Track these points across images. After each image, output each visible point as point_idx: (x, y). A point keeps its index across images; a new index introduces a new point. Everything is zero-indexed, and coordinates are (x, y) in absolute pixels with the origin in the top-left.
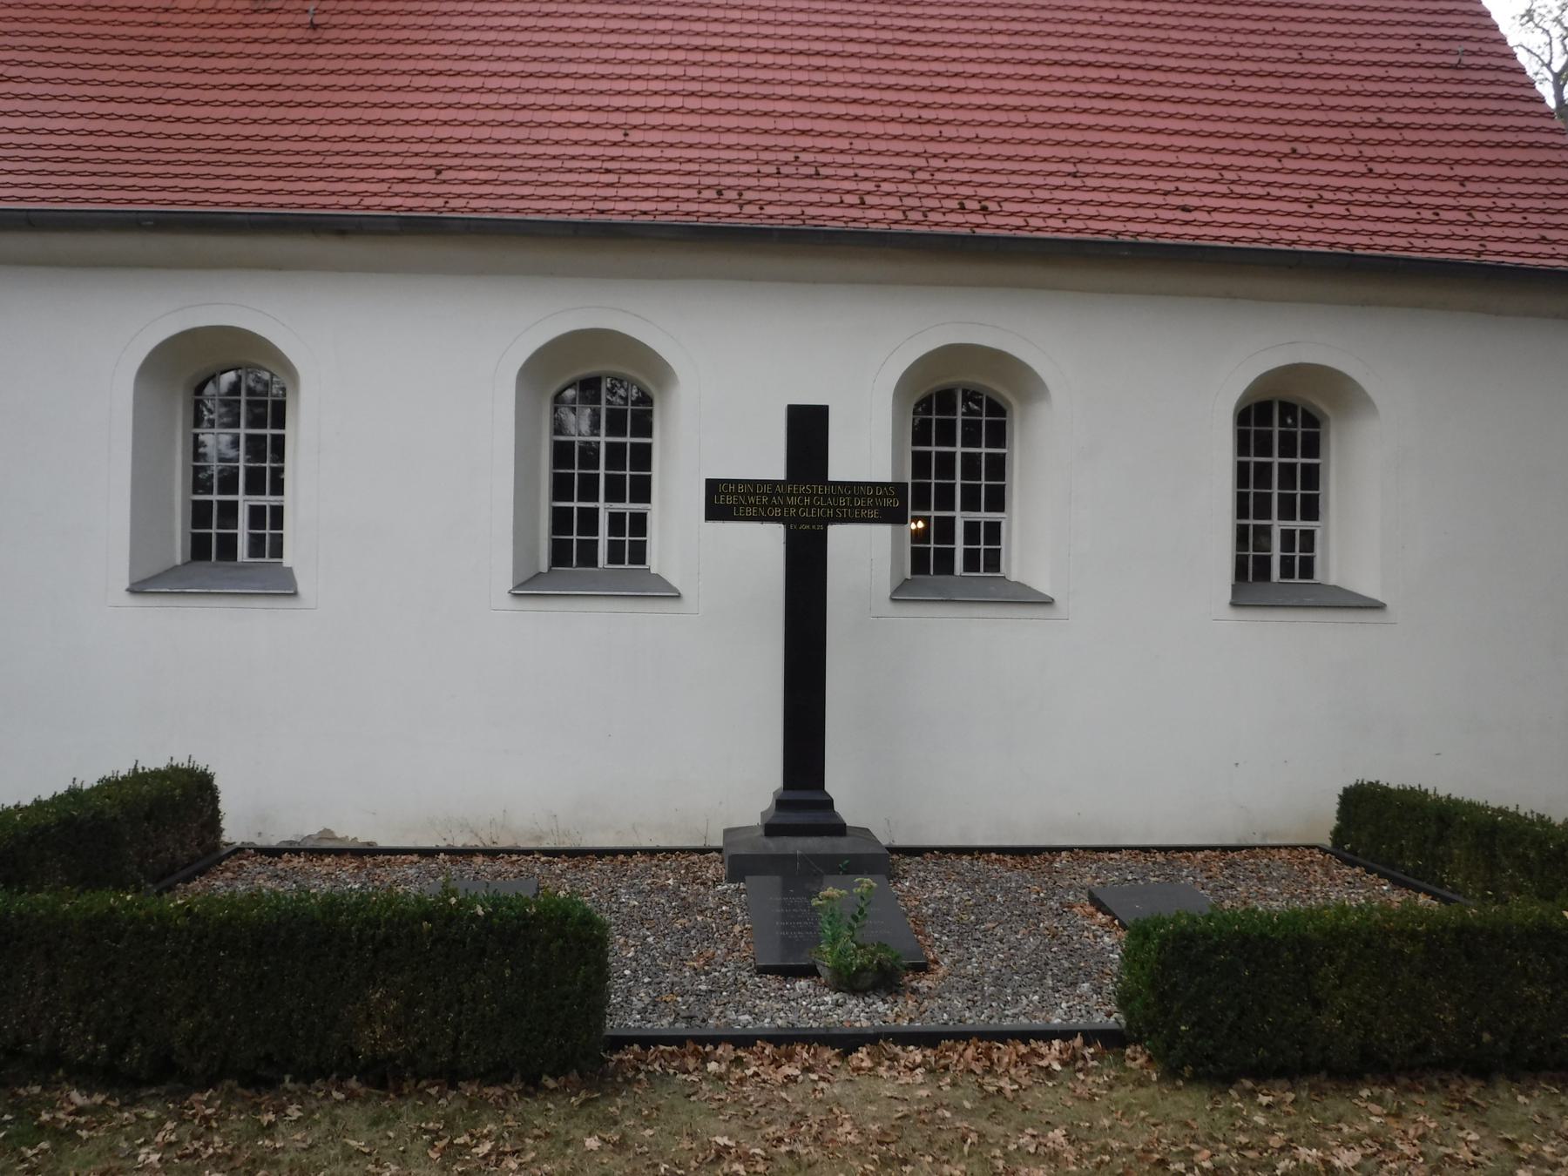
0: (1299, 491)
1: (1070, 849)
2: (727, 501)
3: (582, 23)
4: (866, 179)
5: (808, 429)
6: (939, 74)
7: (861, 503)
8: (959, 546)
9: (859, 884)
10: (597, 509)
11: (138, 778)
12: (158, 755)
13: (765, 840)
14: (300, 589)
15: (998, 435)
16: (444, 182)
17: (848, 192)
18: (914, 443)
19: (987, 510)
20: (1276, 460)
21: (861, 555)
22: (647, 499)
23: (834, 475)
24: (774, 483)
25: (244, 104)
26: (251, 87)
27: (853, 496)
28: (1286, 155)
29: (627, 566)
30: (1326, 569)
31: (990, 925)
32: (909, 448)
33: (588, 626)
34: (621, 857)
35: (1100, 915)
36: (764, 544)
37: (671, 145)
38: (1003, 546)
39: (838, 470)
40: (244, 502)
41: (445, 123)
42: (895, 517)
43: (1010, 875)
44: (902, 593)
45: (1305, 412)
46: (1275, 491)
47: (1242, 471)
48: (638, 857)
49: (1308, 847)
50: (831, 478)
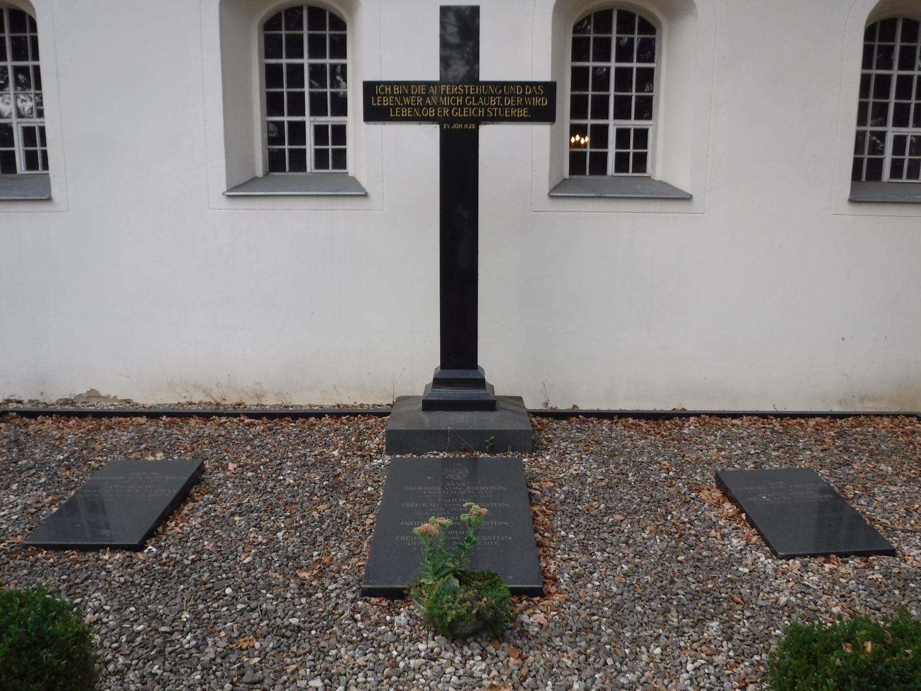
1: (698, 415)
2: (385, 103)
7: (511, 102)
8: (612, 150)
9: (467, 510)
13: (422, 414)
14: (55, 193)
15: (648, 51)
21: (515, 156)
24: (428, 84)
29: (330, 170)
31: (618, 517)
33: (294, 221)
34: (312, 419)
35: (727, 505)
36: (422, 142)
38: (649, 150)
42: (545, 115)
43: (644, 443)
44: (558, 191)
47: (865, 81)
48: (326, 420)
49: (908, 415)
50: (483, 78)
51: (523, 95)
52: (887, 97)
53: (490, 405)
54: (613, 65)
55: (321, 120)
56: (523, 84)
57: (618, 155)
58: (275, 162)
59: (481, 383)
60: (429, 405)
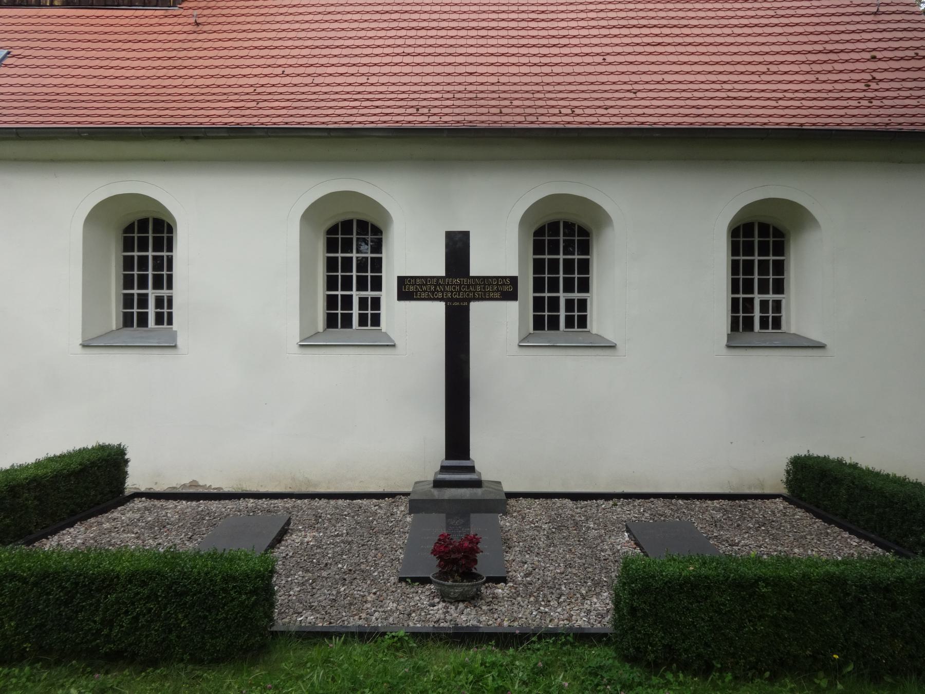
0: (771, 277)
2: (410, 289)
3: (349, 17)
4: (505, 99)
5: (458, 247)
6: (554, 37)
7: (490, 289)
10: (352, 296)
11: (50, 460)
12: (111, 440)
13: (432, 490)
14: (180, 342)
15: (585, 248)
16: (261, 108)
17: (565, 107)
18: (535, 253)
19: (579, 292)
20: (756, 258)
22: (380, 289)
23: (473, 272)
24: (438, 278)
25: (269, 66)
26: (159, 58)
27: (485, 285)
28: (764, 73)
29: (369, 327)
30: (788, 323)
32: (531, 257)
36: (434, 312)
37: (394, 84)
38: (588, 313)
39: (476, 269)
40: (152, 294)
41: (266, 75)
45: (774, 228)
46: (756, 277)
50: (472, 274)
51: (497, 284)
52: (752, 274)
53: (478, 484)
54: (561, 257)
55: (363, 294)
56: (497, 278)
57: (567, 317)
58: (331, 322)
59: (472, 469)
60: (438, 484)
